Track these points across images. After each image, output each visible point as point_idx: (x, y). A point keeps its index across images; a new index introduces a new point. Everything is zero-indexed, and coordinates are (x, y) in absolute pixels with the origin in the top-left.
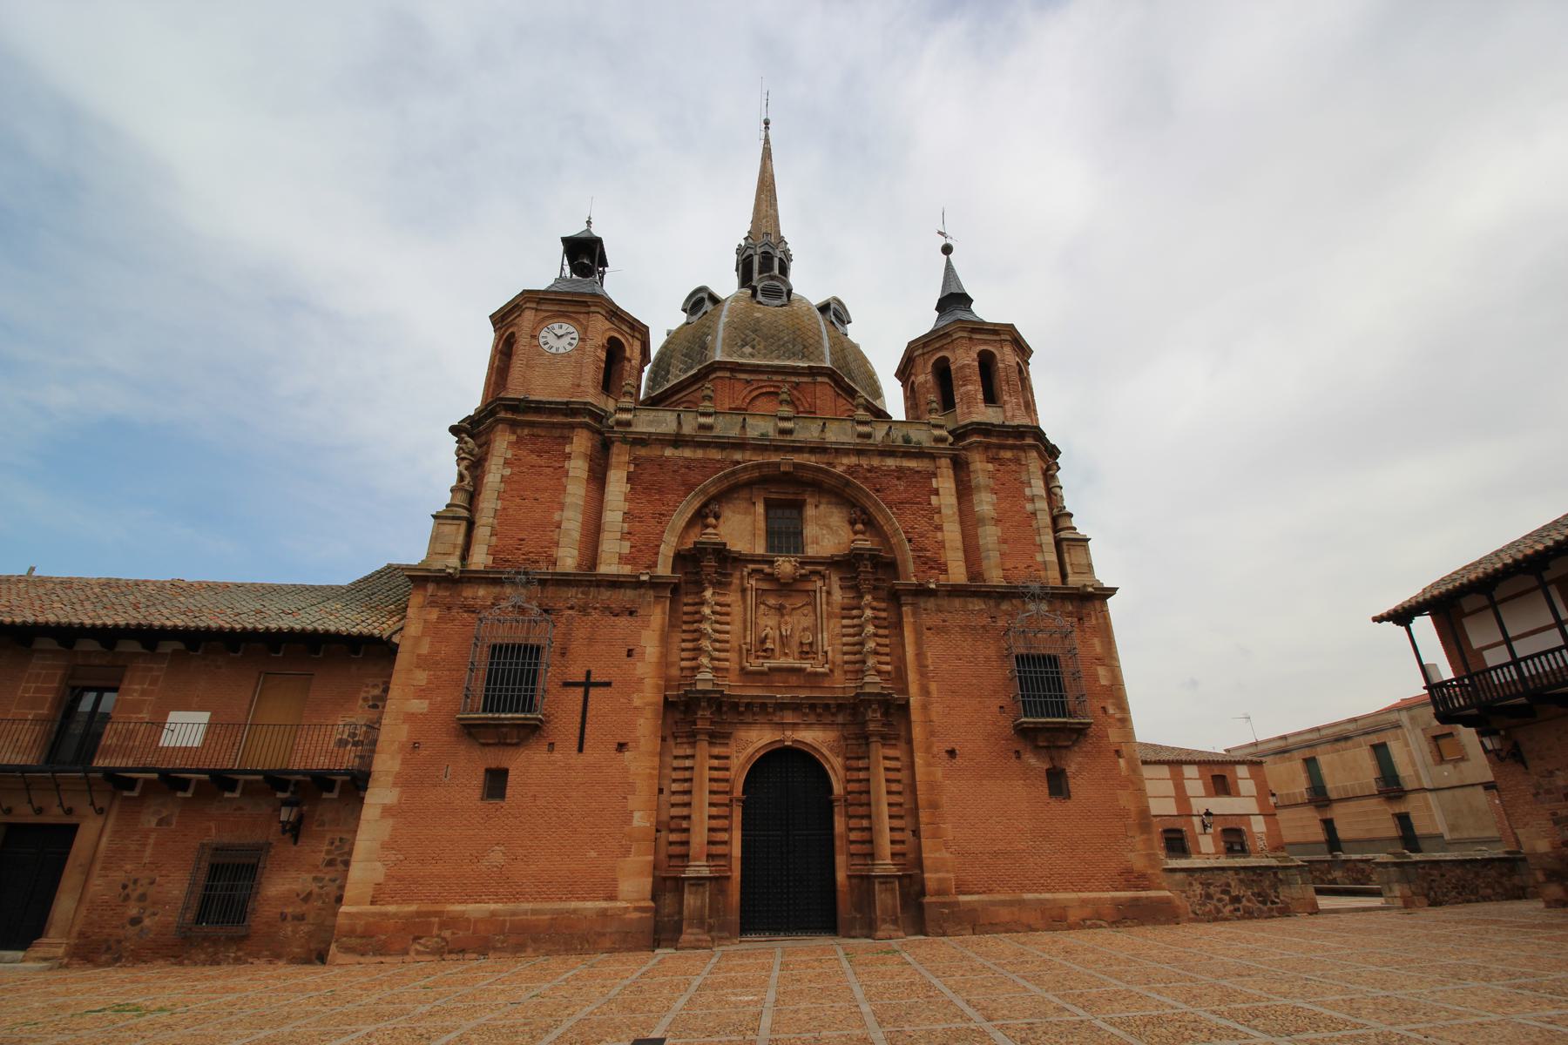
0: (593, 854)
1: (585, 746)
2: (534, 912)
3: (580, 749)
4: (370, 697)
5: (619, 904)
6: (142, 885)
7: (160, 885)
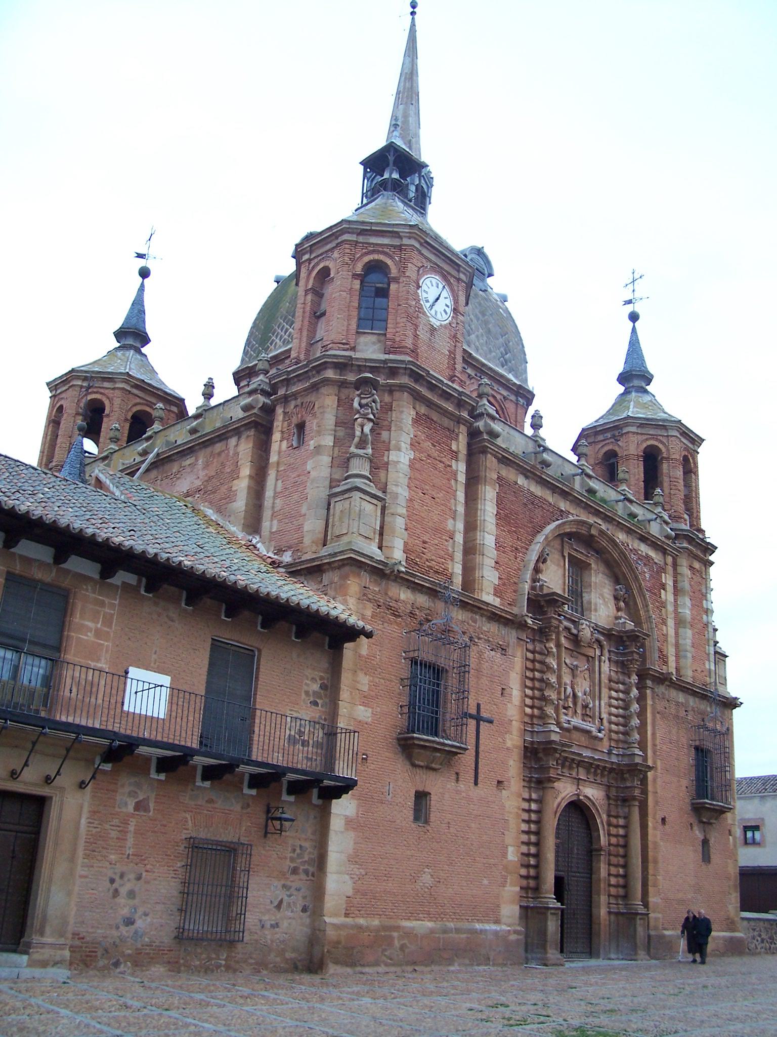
0: (485, 882)
1: (479, 780)
2: (458, 931)
3: (476, 783)
4: (311, 693)
5: (504, 927)
6: (129, 880)
7: (147, 882)
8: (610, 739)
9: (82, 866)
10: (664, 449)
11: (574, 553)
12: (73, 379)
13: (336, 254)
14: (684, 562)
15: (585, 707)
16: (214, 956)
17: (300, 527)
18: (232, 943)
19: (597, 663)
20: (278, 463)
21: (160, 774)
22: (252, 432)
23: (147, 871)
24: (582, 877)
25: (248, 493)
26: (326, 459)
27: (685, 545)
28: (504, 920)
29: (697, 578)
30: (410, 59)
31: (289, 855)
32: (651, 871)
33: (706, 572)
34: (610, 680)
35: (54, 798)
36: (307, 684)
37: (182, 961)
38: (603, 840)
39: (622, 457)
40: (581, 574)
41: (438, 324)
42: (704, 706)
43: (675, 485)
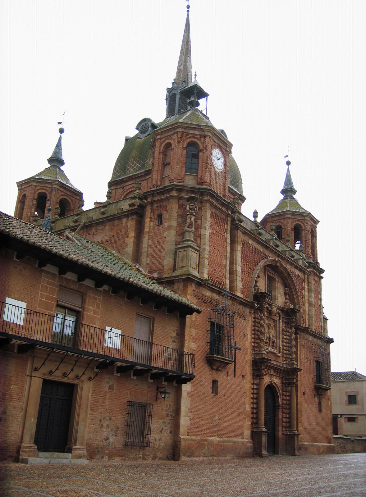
2: (229, 442)
3: (235, 377)
5: (245, 440)
7: (113, 421)
8: (283, 357)
9: (90, 414)
10: (303, 226)
11: (269, 274)
12: (31, 182)
13: (174, 137)
14: (312, 277)
15: (273, 342)
16: (138, 453)
17: (161, 262)
18: (144, 447)
19: (278, 323)
20: (149, 232)
21: (118, 374)
22: (135, 217)
23: (113, 416)
24: (272, 418)
25: (134, 245)
26: (173, 232)
27: (312, 270)
28: (245, 437)
29: (317, 285)
30: (187, 34)
31: (165, 408)
32: (299, 416)
33: (320, 282)
34: (283, 330)
35: (79, 385)
36: (171, 333)
37: (126, 456)
38: (280, 402)
39: (284, 228)
40: (271, 283)
41: (219, 171)
42: (319, 342)
43: (308, 242)
